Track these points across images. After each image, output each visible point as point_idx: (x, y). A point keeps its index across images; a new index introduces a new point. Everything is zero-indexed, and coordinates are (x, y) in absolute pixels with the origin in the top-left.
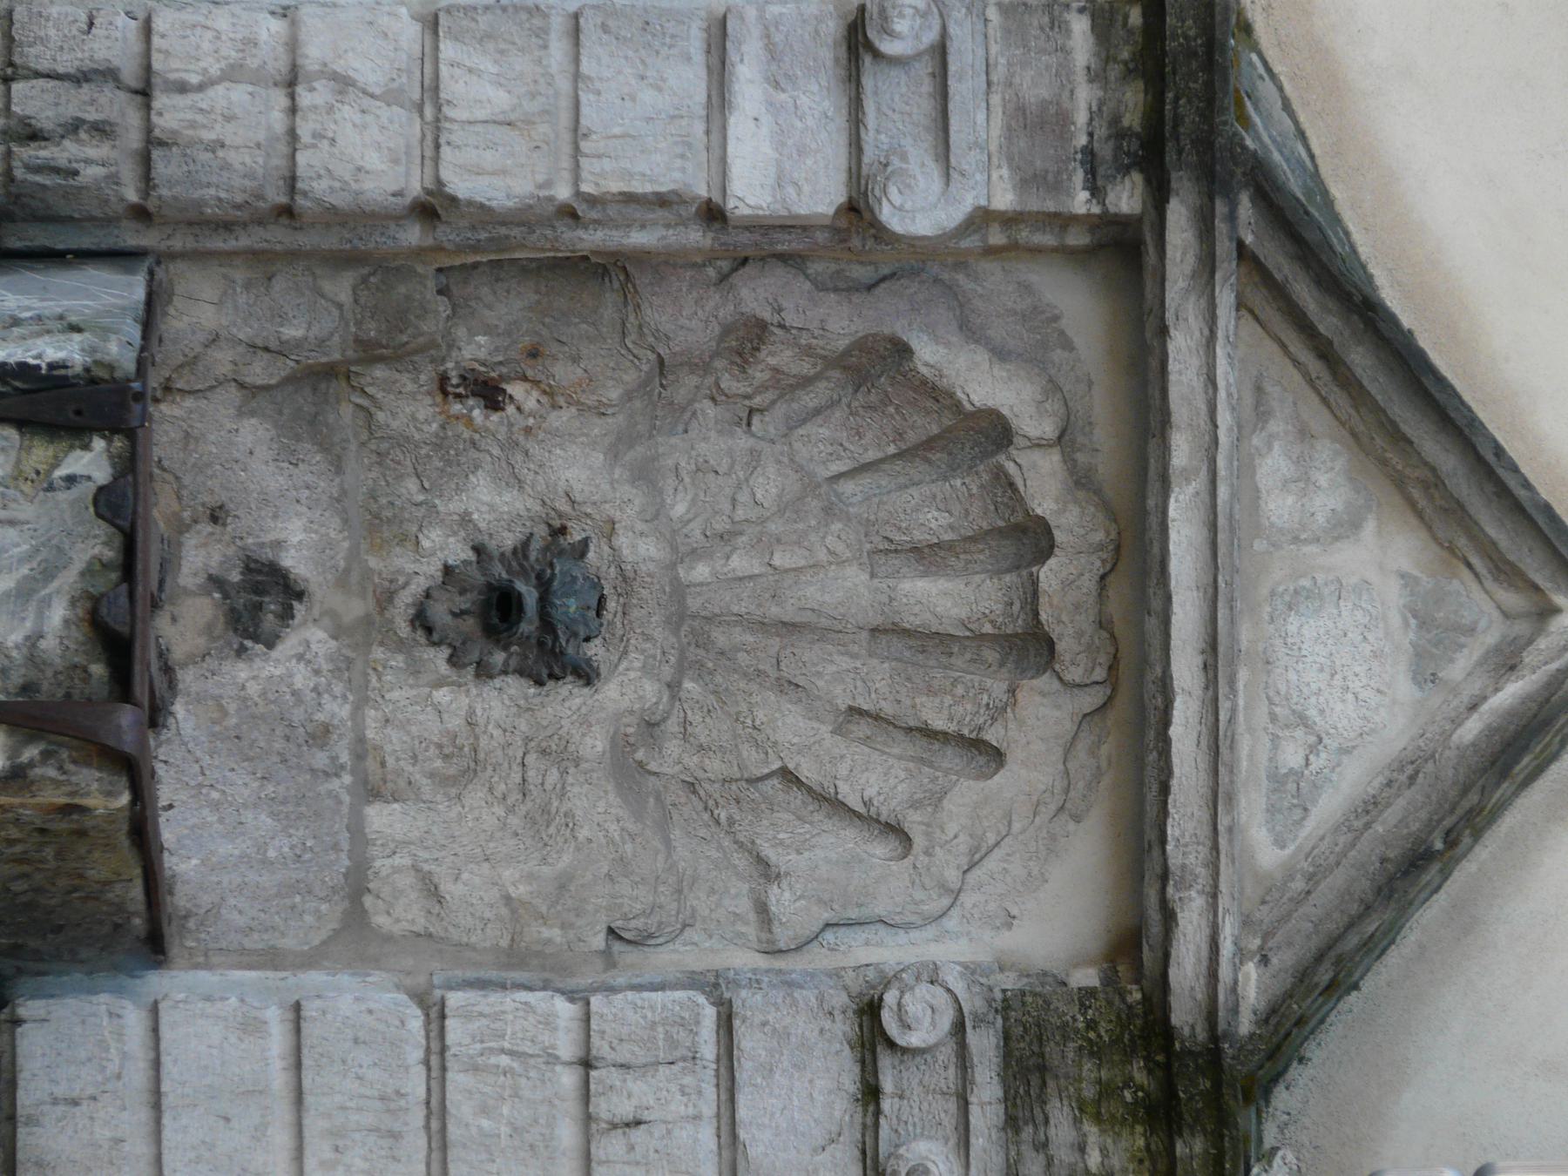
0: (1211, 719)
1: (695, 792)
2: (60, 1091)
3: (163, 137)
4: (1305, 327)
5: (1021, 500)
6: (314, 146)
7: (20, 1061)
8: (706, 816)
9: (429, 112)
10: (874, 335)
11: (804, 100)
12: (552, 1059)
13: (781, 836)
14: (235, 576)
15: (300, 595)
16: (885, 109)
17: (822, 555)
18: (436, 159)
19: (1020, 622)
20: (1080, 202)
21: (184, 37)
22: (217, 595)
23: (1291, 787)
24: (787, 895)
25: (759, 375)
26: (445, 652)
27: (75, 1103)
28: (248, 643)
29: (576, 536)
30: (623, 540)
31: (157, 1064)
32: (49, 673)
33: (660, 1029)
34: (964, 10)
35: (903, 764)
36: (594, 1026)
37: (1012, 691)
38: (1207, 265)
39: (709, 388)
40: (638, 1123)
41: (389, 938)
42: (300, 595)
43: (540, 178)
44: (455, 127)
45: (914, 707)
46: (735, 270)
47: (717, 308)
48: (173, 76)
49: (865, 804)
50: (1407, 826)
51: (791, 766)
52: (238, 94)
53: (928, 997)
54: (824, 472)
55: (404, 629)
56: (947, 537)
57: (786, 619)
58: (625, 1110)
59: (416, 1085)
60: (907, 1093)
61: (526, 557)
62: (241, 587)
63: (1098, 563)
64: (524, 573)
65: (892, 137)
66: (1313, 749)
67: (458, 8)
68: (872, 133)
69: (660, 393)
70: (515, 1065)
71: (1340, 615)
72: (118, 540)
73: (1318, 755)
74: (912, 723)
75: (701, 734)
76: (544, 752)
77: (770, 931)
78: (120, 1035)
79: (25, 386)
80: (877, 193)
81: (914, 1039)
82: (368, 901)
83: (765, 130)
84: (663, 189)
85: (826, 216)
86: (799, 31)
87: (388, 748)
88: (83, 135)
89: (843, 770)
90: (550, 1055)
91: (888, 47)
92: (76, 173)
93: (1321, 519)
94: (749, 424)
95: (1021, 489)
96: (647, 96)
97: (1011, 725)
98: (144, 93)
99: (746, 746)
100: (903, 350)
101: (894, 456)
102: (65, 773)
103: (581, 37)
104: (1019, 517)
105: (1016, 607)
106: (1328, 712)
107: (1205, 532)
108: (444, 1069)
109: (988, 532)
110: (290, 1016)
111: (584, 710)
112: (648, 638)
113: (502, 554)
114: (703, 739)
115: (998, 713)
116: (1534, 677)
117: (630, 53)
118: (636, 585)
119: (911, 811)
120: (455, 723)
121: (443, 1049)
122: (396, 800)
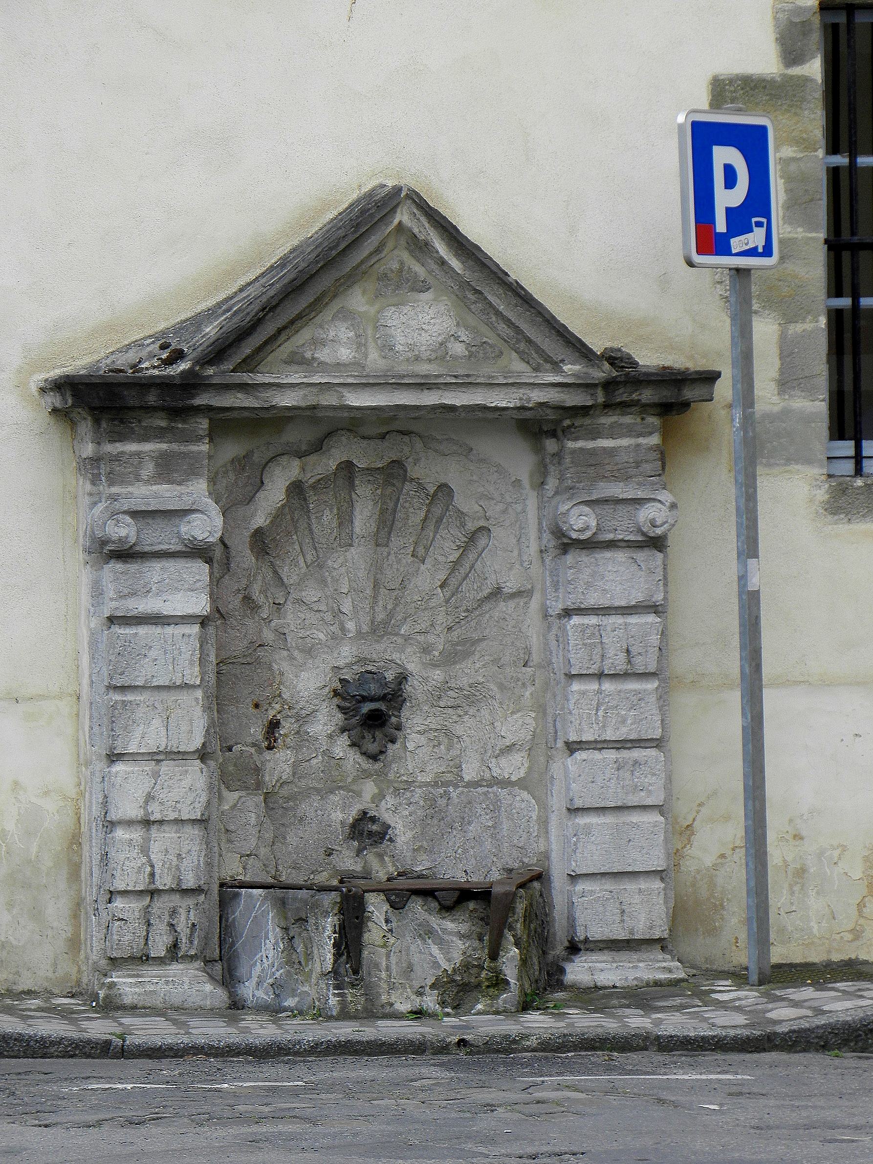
1: (451, 628)
2: (618, 918)
6: (179, 811)
7: (604, 938)
9: (161, 757)
12: (599, 692)
14: (356, 843)
15: (365, 813)
16: (159, 541)
17: (343, 570)
18: (185, 753)
19: (378, 477)
23: (474, 349)
24: (508, 584)
26: (390, 745)
27: (623, 912)
28: (388, 837)
30: (341, 663)
31: (603, 874)
32: (473, 928)
36: (585, 672)
38: (243, 387)
41: (530, 768)
42: (365, 813)
43: (194, 703)
45: (413, 526)
47: (236, 620)
53: (575, 518)
55: (378, 766)
56: (335, 511)
58: (622, 656)
59: (611, 755)
60: (614, 527)
63: (355, 440)
64: (356, 710)
65: (173, 537)
66: (457, 338)
68: (171, 547)
69: (270, 646)
77: (524, 592)
81: (593, 523)
82: (514, 778)
83: (170, 598)
86: (122, 581)
87: (436, 770)
88: (174, 922)
89: (441, 559)
90: (598, 692)
92: (194, 925)
93: (352, 334)
94: (279, 604)
95: (322, 476)
96: (153, 654)
98: (153, 893)
100: (259, 535)
105: (371, 478)
108: (605, 741)
112: (385, 650)
113: (346, 719)
115: (421, 487)
119: (466, 527)
120: (423, 740)
121: (596, 742)
122: (460, 766)
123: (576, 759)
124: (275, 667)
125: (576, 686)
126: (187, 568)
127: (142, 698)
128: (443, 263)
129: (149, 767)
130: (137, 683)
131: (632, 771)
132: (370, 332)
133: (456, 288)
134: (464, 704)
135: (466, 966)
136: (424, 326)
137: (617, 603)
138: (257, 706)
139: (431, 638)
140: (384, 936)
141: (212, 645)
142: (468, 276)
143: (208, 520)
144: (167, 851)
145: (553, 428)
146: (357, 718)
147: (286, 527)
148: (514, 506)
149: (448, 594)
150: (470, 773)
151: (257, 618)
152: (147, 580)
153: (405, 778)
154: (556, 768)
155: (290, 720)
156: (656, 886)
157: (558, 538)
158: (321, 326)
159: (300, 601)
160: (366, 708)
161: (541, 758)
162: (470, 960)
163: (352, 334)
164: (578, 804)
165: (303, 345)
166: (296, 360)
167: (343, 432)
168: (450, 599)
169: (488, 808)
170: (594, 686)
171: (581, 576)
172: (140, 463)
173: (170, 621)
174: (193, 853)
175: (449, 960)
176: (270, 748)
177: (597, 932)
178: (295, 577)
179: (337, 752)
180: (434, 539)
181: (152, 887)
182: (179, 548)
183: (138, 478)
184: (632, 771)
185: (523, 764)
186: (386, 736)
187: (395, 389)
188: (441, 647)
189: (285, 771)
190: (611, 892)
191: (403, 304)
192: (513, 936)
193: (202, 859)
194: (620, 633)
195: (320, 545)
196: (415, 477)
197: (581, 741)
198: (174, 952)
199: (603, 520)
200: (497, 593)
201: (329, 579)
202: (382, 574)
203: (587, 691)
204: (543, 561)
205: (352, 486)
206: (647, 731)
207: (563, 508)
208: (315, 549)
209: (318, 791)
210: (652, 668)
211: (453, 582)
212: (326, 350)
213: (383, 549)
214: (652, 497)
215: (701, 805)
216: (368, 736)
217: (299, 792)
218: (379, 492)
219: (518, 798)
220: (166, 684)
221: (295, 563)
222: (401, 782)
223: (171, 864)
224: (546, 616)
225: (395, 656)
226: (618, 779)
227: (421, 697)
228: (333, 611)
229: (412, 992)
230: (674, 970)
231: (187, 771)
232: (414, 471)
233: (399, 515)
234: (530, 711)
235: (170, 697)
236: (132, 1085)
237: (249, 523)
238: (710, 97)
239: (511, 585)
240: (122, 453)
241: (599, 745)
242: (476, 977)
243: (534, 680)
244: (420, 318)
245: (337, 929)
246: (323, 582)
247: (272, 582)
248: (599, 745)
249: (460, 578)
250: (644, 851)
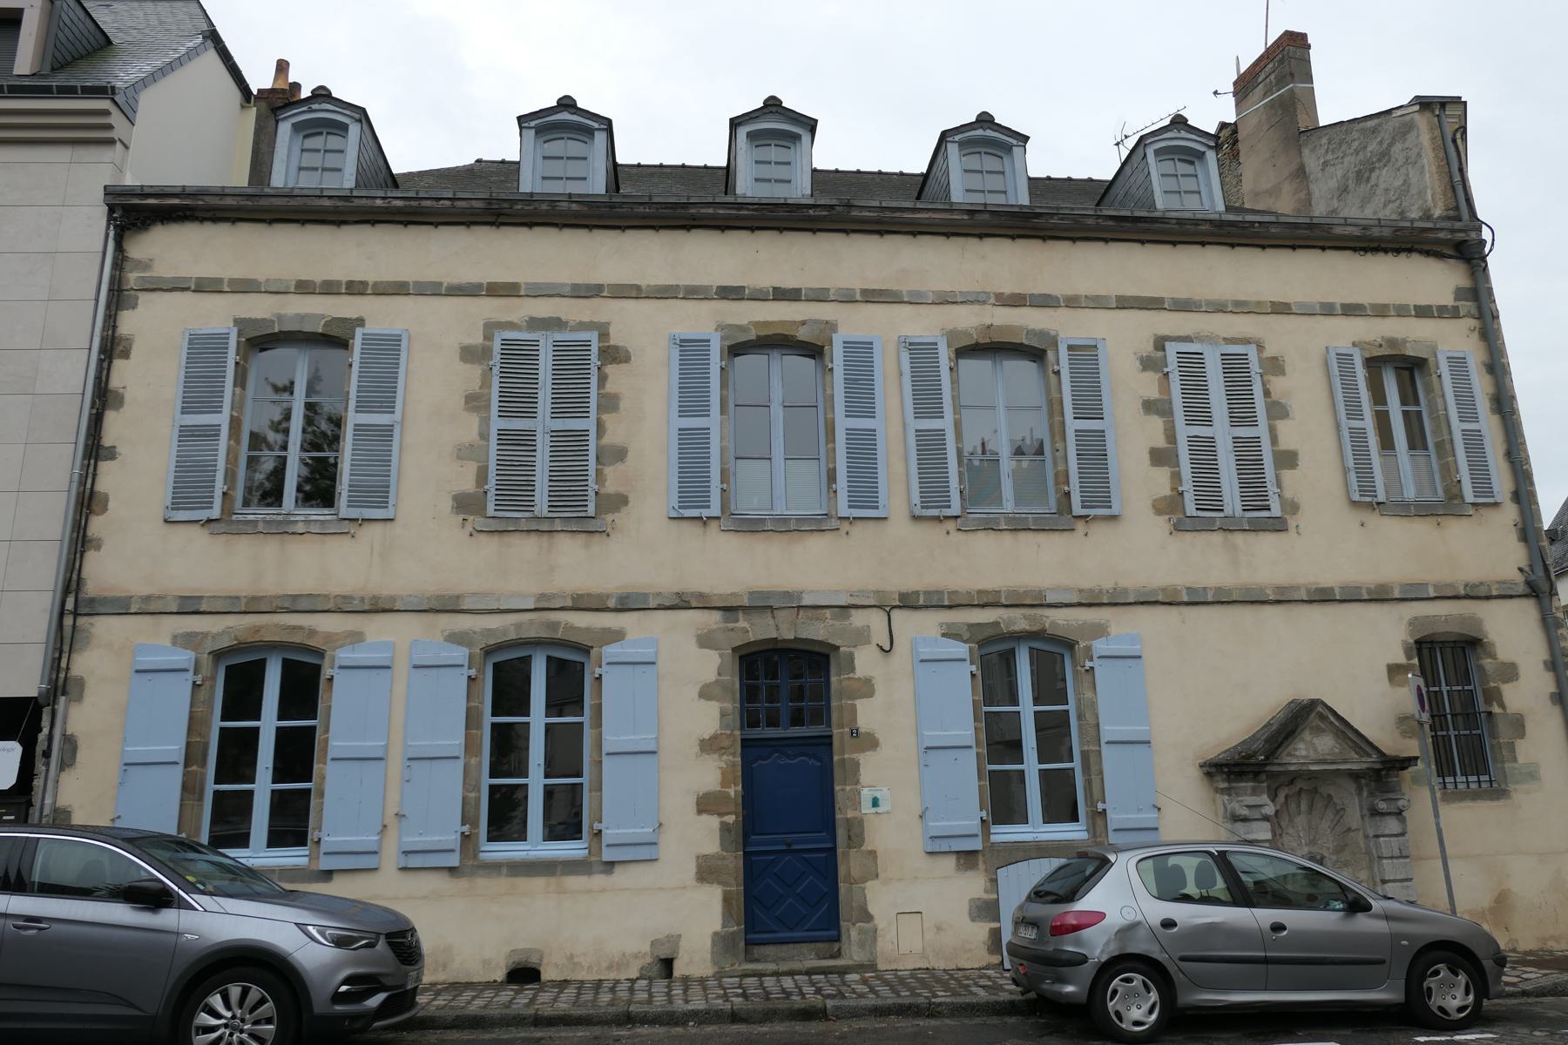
59: (1398, 884)
125: (1385, 861)
159: (1287, 834)
166: (1289, 755)
183: (1246, 794)
200: (1349, 830)
232: (1320, 791)
236: (737, 625)
246: (1293, 827)
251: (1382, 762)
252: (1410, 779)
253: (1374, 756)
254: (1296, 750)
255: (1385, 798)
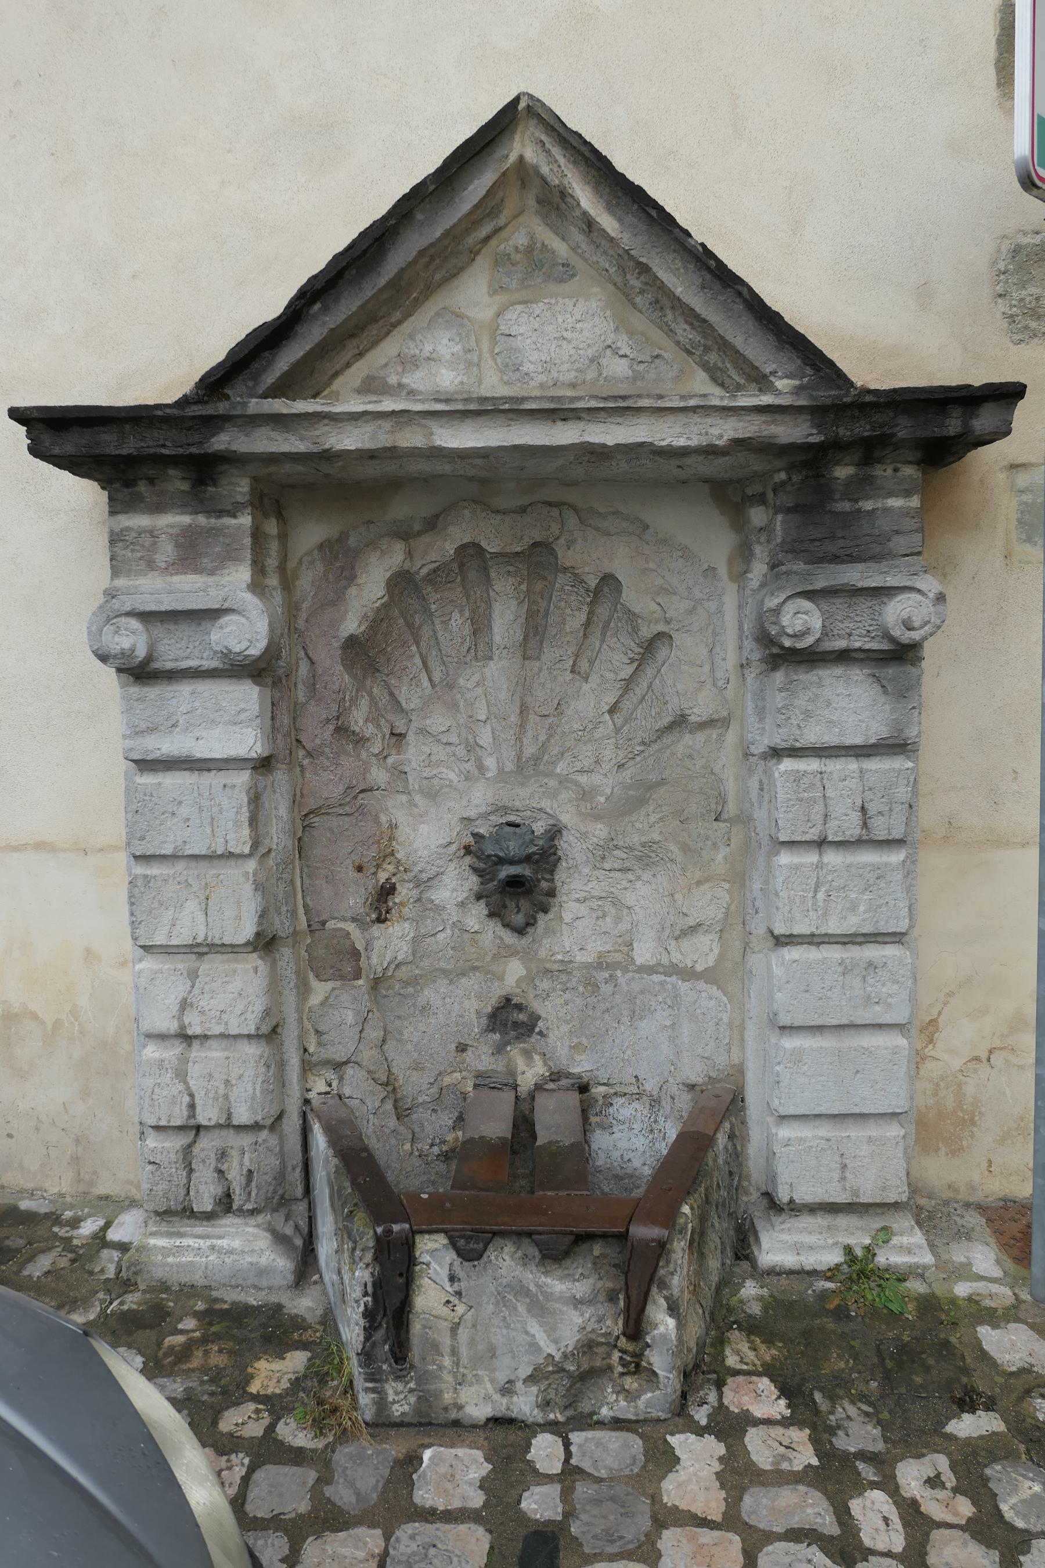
0: (603, 414)
1: (623, 765)
2: (836, 1175)
3: (225, 1116)
4: (323, 351)
5: (445, 565)
6: (226, 1024)
8: (638, 759)
10: (342, 660)
11: (184, 708)
12: (820, 866)
13: (653, 714)
14: (497, 1037)
15: (508, 1000)
17: (479, 691)
18: (232, 946)
20: (245, 520)
21: (160, 1106)
22: (509, 1048)
23: (641, 367)
24: (695, 710)
25: (370, 730)
26: (540, 916)
28: (537, 1030)
29: (470, 840)
30: (472, 813)
31: (818, 1116)
33: (801, 795)
34: (114, 601)
35: (608, 638)
36: (798, 839)
37: (565, 570)
38: (279, 421)
39: (379, 760)
40: (863, 809)
41: (721, 956)
43: (242, 880)
44: (210, 934)
45: (572, 632)
46: (304, 747)
47: (328, 759)
48: (185, 1113)
49: (632, 662)
50: (678, 269)
51: (607, 708)
52: (194, 1071)
54: (429, 690)
56: (467, 614)
57: (518, 711)
58: (856, 817)
59: (834, 953)
60: (848, 631)
61: (484, 870)
62: (503, 1033)
63: (484, 514)
66: (616, 352)
67: (133, 933)
68: (204, 662)
70: (823, 889)
71: (522, 334)
72: (498, 1241)
73: (619, 348)
74: (581, 634)
75: (586, 763)
76: (603, 858)
77: (717, 721)
78: (801, 1140)
79: (382, 1312)
80: (240, 658)
82: (699, 968)
83: (204, 734)
84: (246, 800)
85: (260, 691)
88: (224, 1167)
89: (609, 676)
90: (817, 867)
91: (141, 653)
92: (250, 1171)
93: (457, 348)
95: (437, 564)
96: (184, 811)
97: (587, 570)
99: (595, 734)
100: (352, 642)
101: (418, 647)
102: (675, 1270)
103: (149, 853)
104: (455, 566)
105: (511, 569)
106: (589, 341)
107: (469, 421)
108: (826, 935)
109: (464, 588)
110: (787, 1032)
111: (578, 835)
113: (482, 883)
114: (591, 761)
115: (578, 580)
116: (569, 176)
117: (157, 822)
118: (500, 804)
119: (640, 633)
120: (583, 910)
121: (813, 935)
122: (631, 944)
123: (783, 958)
124: (383, 819)
125: (785, 858)
126: (227, 692)
127: (172, 872)
128: (589, 225)
129: (182, 964)
130: (163, 852)
131: (864, 977)
132: (485, 345)
133: (612, 270)
134: (636, 867)
135: (588, 1346)
136: (565, 334)
137: (848, 741)
138: (360, 869)
139: (596, 779)
140: (448, 1302)
141: (282, 795)
142: (626, 240)
143: (247, 624)
144: (210, 1075)
145: (761, 490)
146: (495, 883)
147: (400, 636)
148: (706, 604)
149: (619, 722)
150: (644, 953)
151: (364, 755)
152: (172, 710)
153: (560, 957)
154: (756, 961)
155: (407, 885)
156: (893, 1134)
157: (767, 646)
158: (411, 337)
159: (423, 731)
160: (506, 871)
161: (737, 943)
162: (593, 1336)
163: (457, 348)
164: (785, 1020)
165: (386, 365)
167: (466, 504)
168: (622, 727)
169: (665, 1003)
170: (811, 858)
171: (796, 702)
172: (155, 543)
173: (211, 765)
174: (246, 1079)
175: (556, 1341)
176: (380, 920)
177: (806, 1194)
178: (418, 701)
179: (471, 924)
180: (600, 649)
181: (192, 1122)
182: (215, 664)
183: (151, 565)
184: (864, 977)
185: (711, 950)
186: (535, 905)
187: (511, 420)
188: (608, 791)
189: (403, 950)
190: (828, 1140)
191: (535, 301)
192: (666, 1298)
193: (258, 1088)
194: (853, 783)
195: (449, 659)
196: (569, 565)
197: (791, 935)
198: (225, 1204)
199: (831, 621)
200: (680, 722)
201: (462, 703)
202: (532, 695)
203: (802, 865)
204: (744, 680)
205: (488, 580)
206: (887, 922)
207: (772, 603)
208: (444, 663)
209: (445, 972)
210: (897, 834)
211: (626, 705)
212: (419, 374)
213: (533, 663)
214: (908, 584)
215: (951, 994)
216: (511, 905)
217: (421, 976)
218: (524, 587)
219: (704, 995)
220: (203, 853)
221: (414, 680)
222: (555, 962)
223: (216, 1092)
224: (747, 755)
225: (545, 804)
226: (843, 987)
227: (580, 857)
228: (467, 744)
229: (494, 1389)
230: (917, 1251)
231: (235, 971)
232: (567, 557)
233: (552, 618)
234: (724, 880)
235: (211, 871)
237: (338, 630)
238: (998, 31)
239: (700, 709)
240: (128, 529)
241: (814, 940)
242: (604, 1359)
243: (729, 839)
244: (560, 320)
245: (370, 1289)
246: (454, 706)
247: (389, 707)
248: (814, 940)
249: (635, 700)
250: (877, 1087)
251: (818, 412)
252: (1014, 516)
253: (781, 384)
254: (409, 363)
255: (820, 584)
